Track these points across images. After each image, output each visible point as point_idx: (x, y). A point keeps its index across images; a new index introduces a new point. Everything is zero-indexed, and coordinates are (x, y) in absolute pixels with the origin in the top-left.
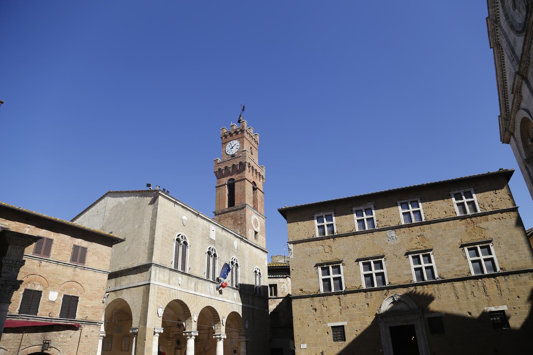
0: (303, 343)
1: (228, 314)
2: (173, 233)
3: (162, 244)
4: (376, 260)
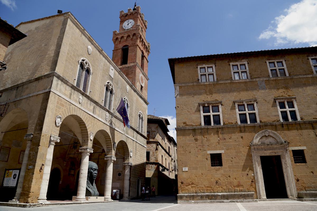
0: (185, 167)
3: (67, 60)
4: (249, 103)
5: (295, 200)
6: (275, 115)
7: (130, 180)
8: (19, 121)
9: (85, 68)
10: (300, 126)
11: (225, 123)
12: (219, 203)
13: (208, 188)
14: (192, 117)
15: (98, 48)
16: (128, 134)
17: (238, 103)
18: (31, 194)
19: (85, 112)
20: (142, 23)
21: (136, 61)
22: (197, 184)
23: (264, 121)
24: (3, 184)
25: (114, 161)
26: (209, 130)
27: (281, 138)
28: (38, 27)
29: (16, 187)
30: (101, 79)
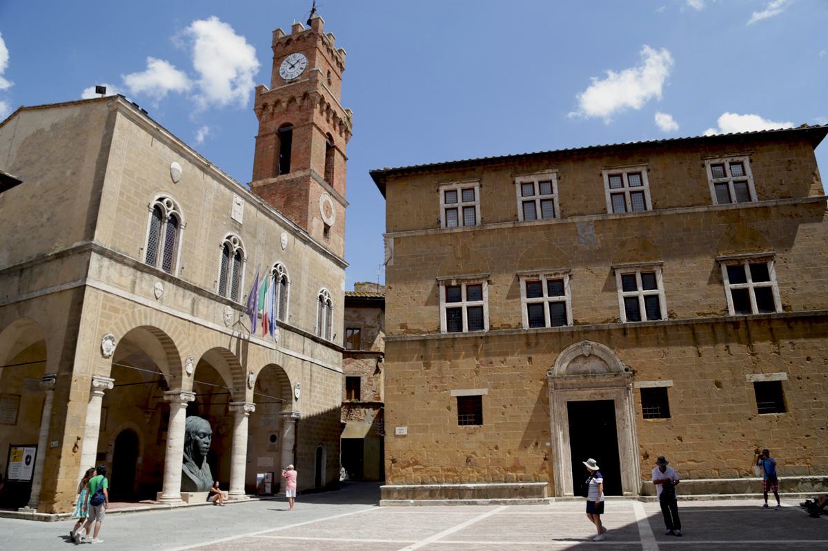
0: (402, 425)
1: (261, 368)
2: (149, 193)
4: (553, 277)
5: (634, 499)
6: (611, 305)
7: (294, 450)
8: (32, 340)
9: (165, 218)
10: (665, 332)
11: (495, 326)
12: (466, 506)
13: (449, 473)
14: (419, 311)
15: (198, 162)
16: (287, 347)
17: (526, 278)
18: (58, 497)
19: (171, 315)
20: (329, 59)
21: (309, 165)
22: (425, 464)
23: (583, 320)
24: (7, 475)
25: (250, 412)
26: (456, 342)
27: (618, 360)
28: (56, 124)
29: (31, 481)
30: (210, 233)
